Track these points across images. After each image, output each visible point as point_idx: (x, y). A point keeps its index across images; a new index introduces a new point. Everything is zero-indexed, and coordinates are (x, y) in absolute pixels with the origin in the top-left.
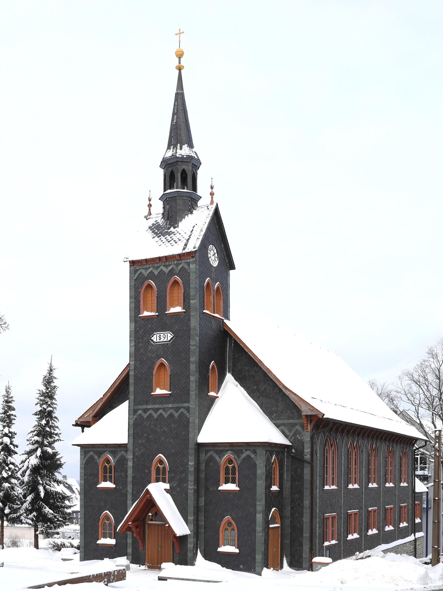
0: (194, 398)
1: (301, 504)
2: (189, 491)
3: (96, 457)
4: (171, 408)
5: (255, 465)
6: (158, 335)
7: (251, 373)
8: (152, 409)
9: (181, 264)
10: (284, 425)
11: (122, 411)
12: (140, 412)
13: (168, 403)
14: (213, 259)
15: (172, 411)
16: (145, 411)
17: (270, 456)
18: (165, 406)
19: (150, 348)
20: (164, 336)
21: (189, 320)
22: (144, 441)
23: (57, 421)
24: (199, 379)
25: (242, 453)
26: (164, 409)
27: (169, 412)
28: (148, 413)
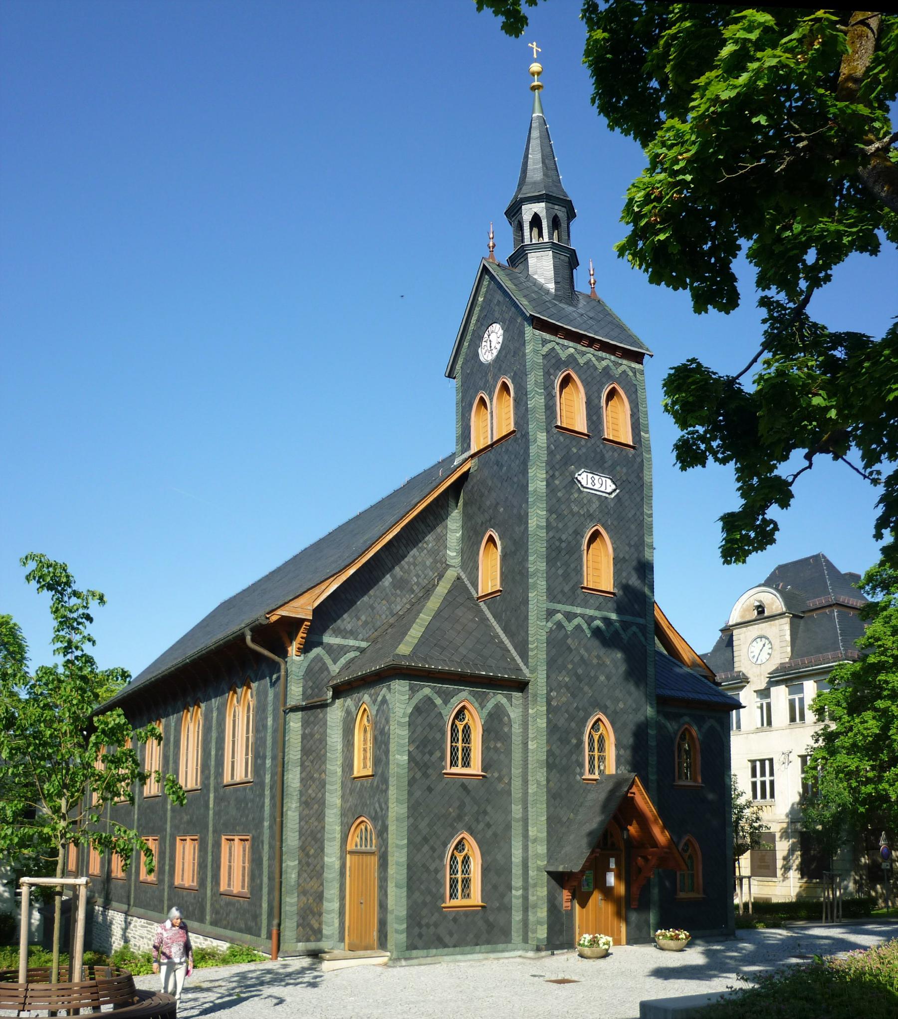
1: (376, 733)
3: (438, 701)
8: (582, 616)
12: (559, 616)
19: (576, 495)
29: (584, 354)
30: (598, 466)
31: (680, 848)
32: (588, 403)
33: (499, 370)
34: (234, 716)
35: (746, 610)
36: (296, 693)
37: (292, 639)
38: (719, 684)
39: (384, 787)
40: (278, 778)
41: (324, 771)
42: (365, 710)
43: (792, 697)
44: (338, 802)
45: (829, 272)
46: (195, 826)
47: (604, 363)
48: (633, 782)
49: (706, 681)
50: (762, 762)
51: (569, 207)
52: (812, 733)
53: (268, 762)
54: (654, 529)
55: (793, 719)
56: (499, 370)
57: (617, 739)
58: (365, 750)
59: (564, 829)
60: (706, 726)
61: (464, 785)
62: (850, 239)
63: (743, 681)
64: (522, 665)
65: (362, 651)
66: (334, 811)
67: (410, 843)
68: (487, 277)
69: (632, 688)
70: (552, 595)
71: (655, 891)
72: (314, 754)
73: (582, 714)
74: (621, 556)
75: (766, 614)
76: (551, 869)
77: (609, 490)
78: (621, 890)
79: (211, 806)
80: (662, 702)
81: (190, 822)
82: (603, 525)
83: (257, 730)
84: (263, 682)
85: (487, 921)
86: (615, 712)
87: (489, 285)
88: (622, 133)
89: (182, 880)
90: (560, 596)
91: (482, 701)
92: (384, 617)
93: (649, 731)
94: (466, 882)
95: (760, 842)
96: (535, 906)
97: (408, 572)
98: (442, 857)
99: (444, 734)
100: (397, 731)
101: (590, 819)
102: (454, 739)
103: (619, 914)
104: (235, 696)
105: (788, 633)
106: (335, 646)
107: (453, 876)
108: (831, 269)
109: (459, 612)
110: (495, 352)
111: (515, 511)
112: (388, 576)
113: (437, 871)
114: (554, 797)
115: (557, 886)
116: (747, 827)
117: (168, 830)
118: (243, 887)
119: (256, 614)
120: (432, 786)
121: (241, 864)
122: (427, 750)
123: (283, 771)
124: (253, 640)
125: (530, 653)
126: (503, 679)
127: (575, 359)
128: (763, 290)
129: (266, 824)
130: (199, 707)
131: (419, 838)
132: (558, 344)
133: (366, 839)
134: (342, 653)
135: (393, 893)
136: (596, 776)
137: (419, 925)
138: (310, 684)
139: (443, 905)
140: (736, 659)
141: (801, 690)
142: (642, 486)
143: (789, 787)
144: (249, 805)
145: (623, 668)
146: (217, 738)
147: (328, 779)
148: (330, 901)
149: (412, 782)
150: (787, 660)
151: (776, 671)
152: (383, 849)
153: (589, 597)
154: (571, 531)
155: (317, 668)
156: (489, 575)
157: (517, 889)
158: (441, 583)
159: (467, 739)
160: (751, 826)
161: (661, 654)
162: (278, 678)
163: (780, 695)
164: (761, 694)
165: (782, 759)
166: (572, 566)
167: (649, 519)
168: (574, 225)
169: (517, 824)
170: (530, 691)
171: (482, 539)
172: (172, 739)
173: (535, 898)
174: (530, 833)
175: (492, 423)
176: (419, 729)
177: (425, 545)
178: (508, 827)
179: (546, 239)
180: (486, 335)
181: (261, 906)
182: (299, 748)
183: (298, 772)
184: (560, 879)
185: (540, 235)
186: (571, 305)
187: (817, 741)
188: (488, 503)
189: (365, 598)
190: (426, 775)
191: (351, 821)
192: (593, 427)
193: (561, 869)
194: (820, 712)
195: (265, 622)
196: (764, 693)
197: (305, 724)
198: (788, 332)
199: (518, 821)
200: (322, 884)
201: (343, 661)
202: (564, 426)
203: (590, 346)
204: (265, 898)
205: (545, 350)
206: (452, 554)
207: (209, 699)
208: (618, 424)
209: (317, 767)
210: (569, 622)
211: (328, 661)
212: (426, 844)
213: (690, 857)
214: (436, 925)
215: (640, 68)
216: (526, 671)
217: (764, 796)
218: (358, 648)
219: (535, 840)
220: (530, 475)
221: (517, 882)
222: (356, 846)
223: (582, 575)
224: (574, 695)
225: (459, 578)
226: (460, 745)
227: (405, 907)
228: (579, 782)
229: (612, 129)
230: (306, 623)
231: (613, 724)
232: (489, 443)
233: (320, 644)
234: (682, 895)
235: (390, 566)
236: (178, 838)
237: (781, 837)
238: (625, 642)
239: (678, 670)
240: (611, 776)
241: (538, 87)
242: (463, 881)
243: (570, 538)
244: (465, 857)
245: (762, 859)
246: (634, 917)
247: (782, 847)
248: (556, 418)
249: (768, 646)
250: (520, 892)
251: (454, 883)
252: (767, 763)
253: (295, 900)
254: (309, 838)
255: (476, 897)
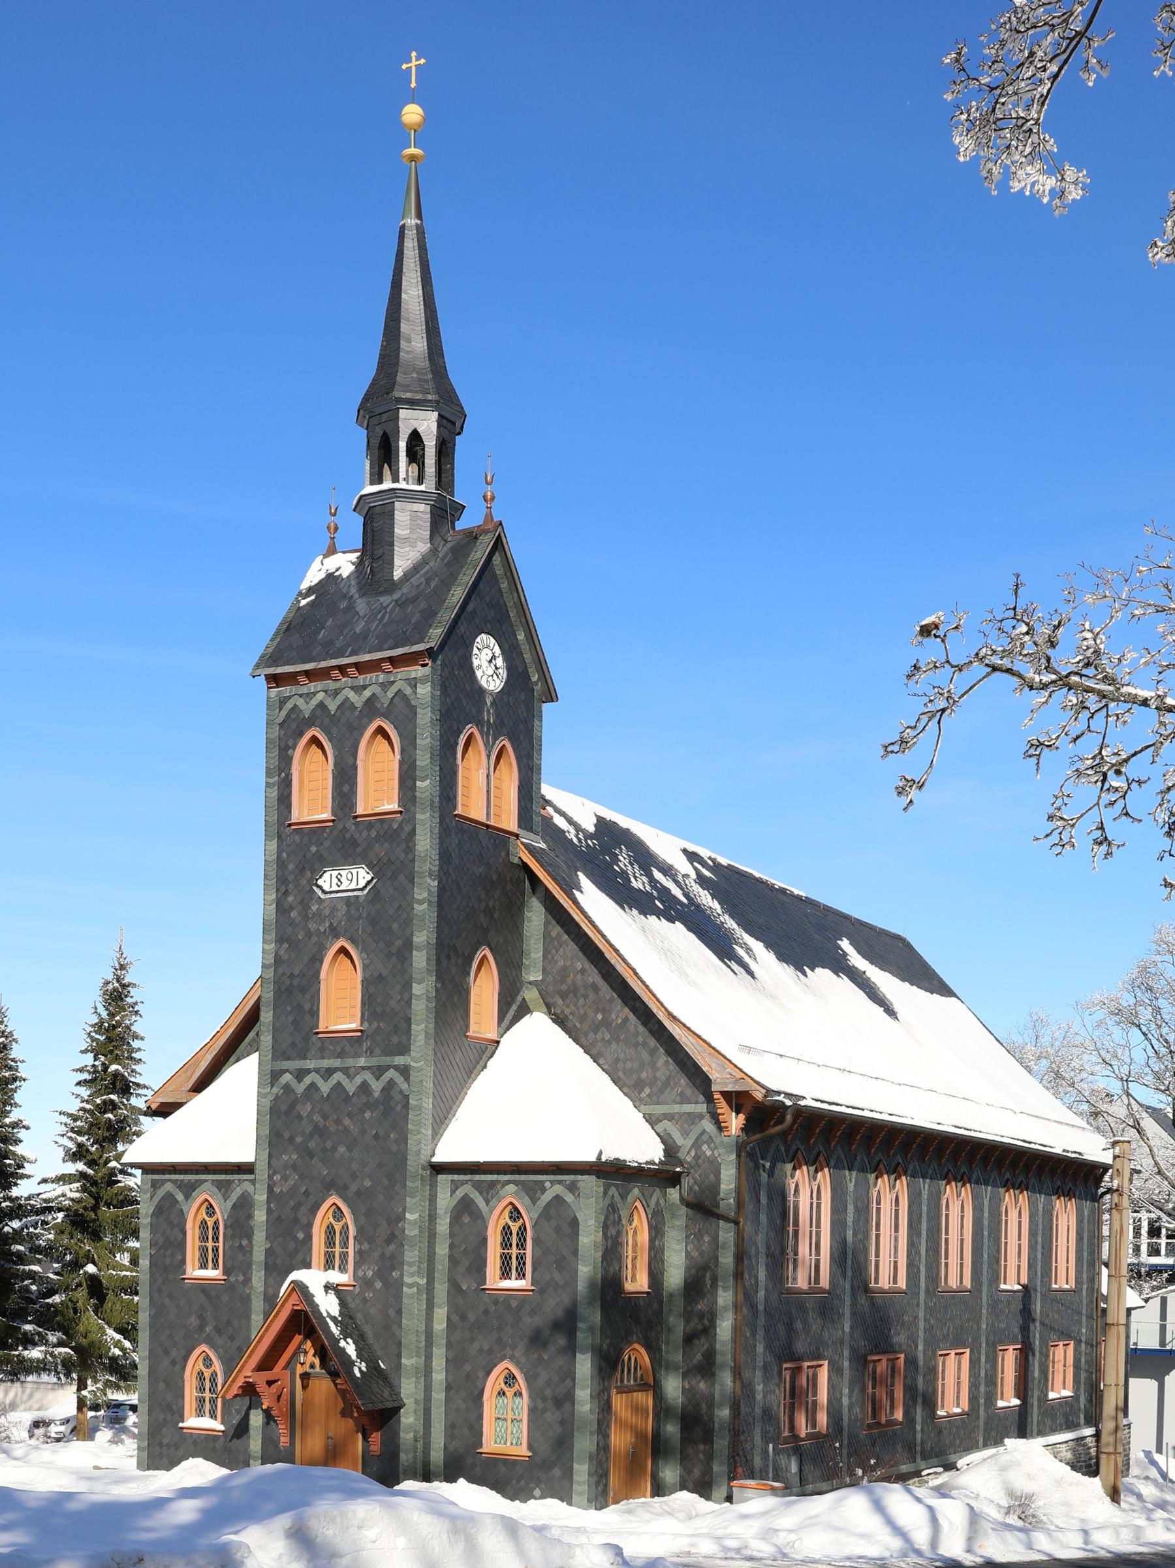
0: (423, 1042)
2: (405, 1289)
3: (180, 1197)
4: (363, 1068)
5: (574, 1223)
6: (335, 873)
7: (590, 979)
8: (317, 1071)
9: (393, 682)
10: (670, 1117)
11: (244, 1074)
12: (287, 1077)
13: (357, 1055)
14: (490, 671)
15: (368, 1076)
16: (300, 1075)
17: (617, 1198)
18: (350, 1062)
19: (314, 908)
20: (350, 877)
21: (413, 833)
22: (295, 1156)
24: (437, 990)
25: (544, 1190)
26: (345, 1071)
27: (358, 1080)
28: (307, 1080)
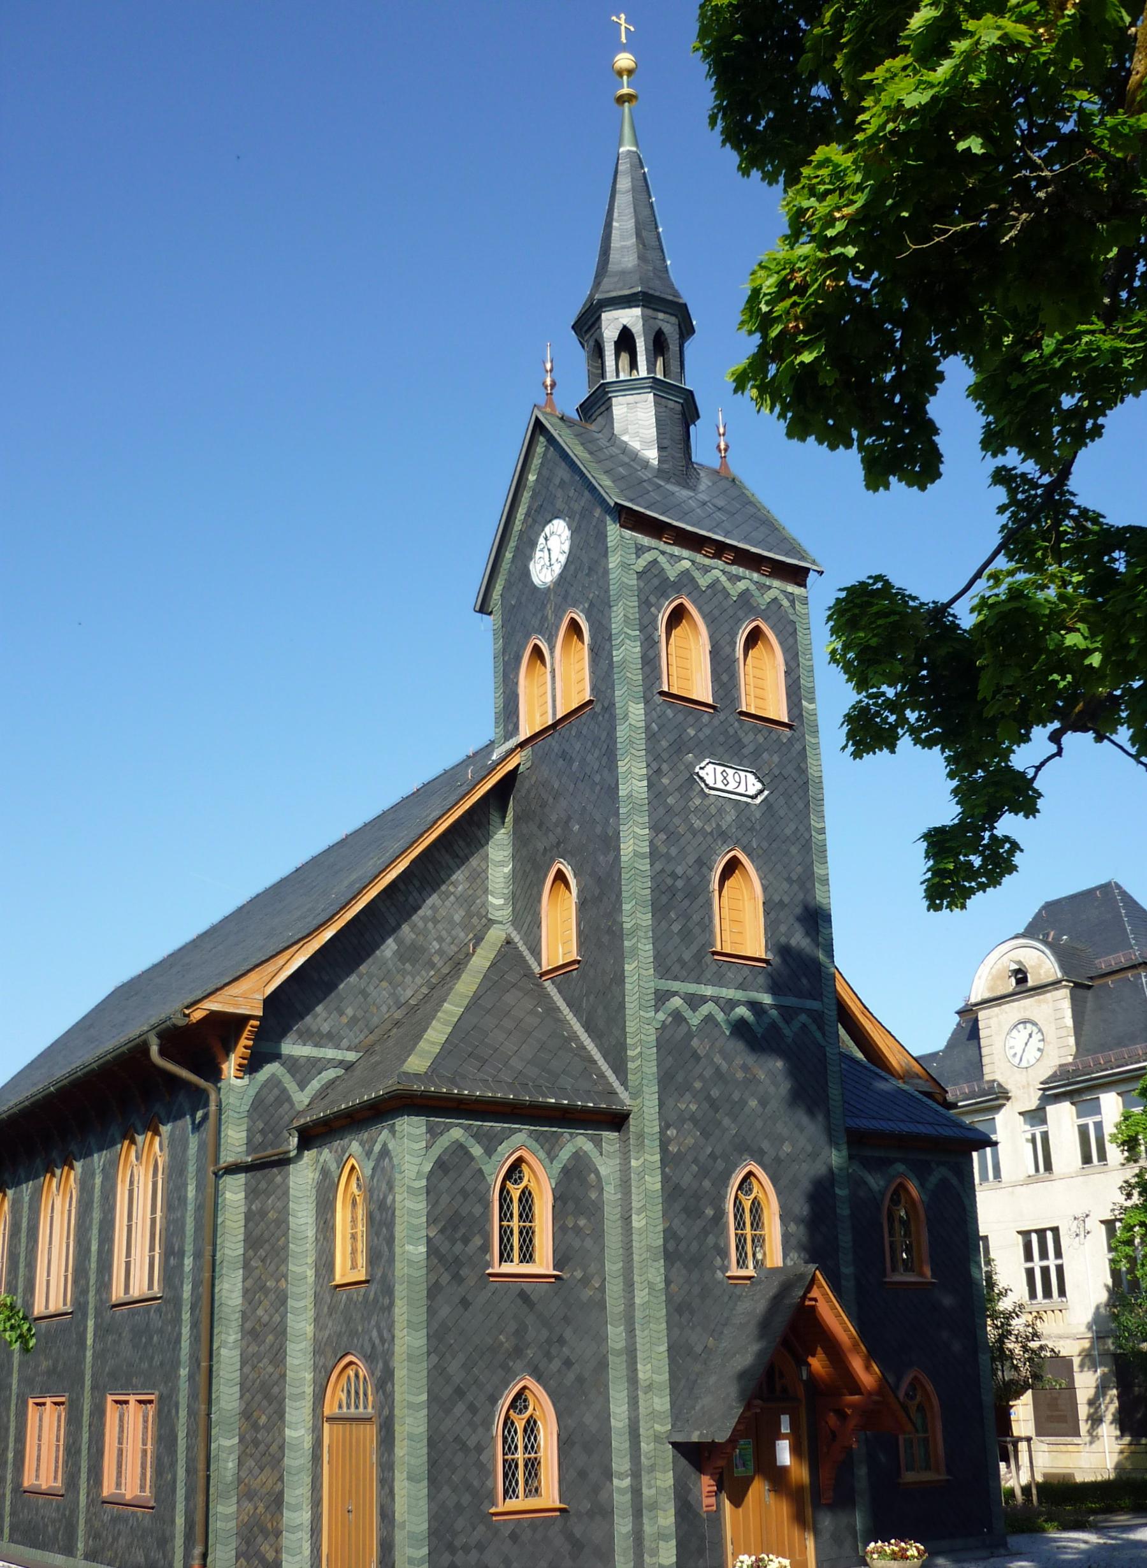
1: (373, 1207)
3: (477, 1150)
8: (716, 1000)
12: (677, 1002)
19: (698, 801)
23: (887, 1076)
28: (705, 1010)
29: (706, 570)
30: (731, 753)
31: (901, 1394)
32: (715, 653)
33: (565, 598)
34: (131, 1183)
35: (996, 978)
36: (235, 1141)
37: (228, 1050)
38: (954, 1106)
39: (387, 1301)
40: (204, 1290)
41: (285, 1276)
42: (353, 1168)
43: (1082, 1121)
44: (310, 1329)
45: (1101, 420)
46: (60, 1380)
47: (742, 585)
48: (814, 1279)
49: (930, 1102)
50: (1041, 1233)
51: (681, 313)
52: (1121, 1184)
53: (188, 1262)
54: (829, 854)
55: (1087, 1159)
56: (565, 598)
57: (783, 1207)
58: (354, 1237)
59: (698, 1367)
60: (933, 1180)
61: (523, 1293)
62: (1132, 361)
63: (998, 1097)
64: (616, 1084)
65: (349, 1067)
66: (303, 1345)
67: (433, 1399)
68: (542, 439)
69: (805, 1120)
70: (663, 967)
71: (862, 1471)
72: (267, 1246)
73: (720, 1165)
74: (777, 898)
75: (1030, 983)
76: (679, 1438)
77: (752, 791)
78: (801, 1474)
79: (89, 1342)
80: (861, 1143)
81: (50, 1372)
82: (744, 850)
83: (169, 1207)
84: (180, 1123)
85: (570, 1537)
86: (778, 1160)
87: (545, 454)
88: (763, 179)
89: (37, 1477)
90: (676, 968)
91: (551, 1149)
92: (384, 1009)
93: (838, 1191)
94: (532, 1467)
95: (1046, 1374)
96: (654, 1507)
97: (424, 933)
98: (488, 1423)
99: (487, 1205)
100: (406, 1203)
101: (742, 1351)
102: (505, 1215)
103: (800, 1519)
104: (133, 1148)
105: (1068, 1013)
106: (302, 1061)
107: (509, 1457)
108: (1105, 415)
109: (510, 998)
110: (557, 569)
111: (598, 830)
112: (390, 941)
113: (480, 1449)
114: (680, 1310)
115: (689, 1469)
116: (1018, 1350)
117: (14, 1387)
118: (143, 1488)
119: (167, 1009)
120: (469, 1298)
121: (140, 1446)
122: (458, 1235)
123: (213, 1278)
124: (162, 1053)
125: (630, 1065)
126: (585, 1110)
127: (693, 580)
128: (994, 455)
129: (184, 1372)
130: (72, 1167)
131: (449, 1390)
132: (663, 553)
133: (357, 1393)
134: (314, 1071)
135: (404, 1492)
136: (750, 1271)
137: (451, 1548)
138: (260, 1125)
139: (493, 1510)
140: (985, 1060)
141: (1097, 1111)
142: (806, 783)
143: (1089, 1277)
144: (155, 1338)
145: (785, 1087)
146: (101, 1222)
147: (291, 1289)
148: (296, 1508)
149: (433, 1291)
150: (1070, 1059)
151: (1053, 1078)
152: (386, 1412)
153: (725, 967)
154: (691, 860)
155: (271, 1098)
156: (559, 938)
157: (621, 1477)
158: (479, 950)
159: (527, 1213)
160: (1025, 1348)
161: (853, 1060)
162: (205, 1117)
163: (1063, 1118)
164: (1032, 1118)
165: (1074, 1228)
166: (696, 918)
167: (820, 837)
168: (690, 346)
169: (617, 1360)
170: (632, 1129)
171: (546, 876)
172: (24, 1225)
173: (653, 1491)
174: (641, 1375)
175: (554, 689)
176: (445, 1199)
177: (452, 889)
178: (602, 1365)
179: (643, 372)
180: (542, 540)
181: (173, 1522)
182: (241, 1237)
183: (240, 1279)
184: (695, 1455)
185: (633, 365)
186: (686, 486)
187: (1129, 1196)
188: (554, 818)
189: (353, 979)
190: (457, 1278)
191: (330, 1364)
192: (722, 693)
193: (695, 1438)
194: (1130, 1144)
195: (182, 1022)
196: (1036, 1116)
197: (252, 1194)
198: (1039, 521)
199: (618, 1353)
200: (281, 1479)
201: (315, 1085)
202: (674, 691)
203: (718, 555)
204: (180, 1507)
205: (641, 563)
206: (498, 902)
207: (89, 1154)
208: (764, 688)
209: (272, 1267)
210: (694, 1010)
211: (291, 1085)
212: (460, 1400)
213: (920, 1408)
214: (481, 1547)
215: (796, 60)
216: (624, 1095)
217: (1047, 1294)
218: (341, 1062)
219: (649, 1388)
220: (620, 770)
221: (620, 1463)
222: (340, 1407)
223: (712, 932)
224: (706, 1134)
225: (509, 942)
226: (515, 1224)
227: (426, 1516)
228: (720, 1283)
229: (746, 173)
230: (252, 1022)
231: (774, 1180)
232: (550, 722)
233: (276, 1056)
234: (909, 1477)
235: (394, 923)
236: (31, 1401)
237: (1082, 1366)
238: (790, 1040)
239: (882, 1086)
240: (774, 1270)
241: (630, 98)
242: (526, 1466)
243: (690, 872)
244: (528, 1422)
245: (1053, 1404)
246: (827, 1521)
247: (1086, 1383)
248: (659, 678)
249: (1037, 1037)
250: (627, 1482)
251: (510, 1468)
252: (1049, 1235)
253: (234, 1508)
254: (259, 1397)
255: (550, 1495)
